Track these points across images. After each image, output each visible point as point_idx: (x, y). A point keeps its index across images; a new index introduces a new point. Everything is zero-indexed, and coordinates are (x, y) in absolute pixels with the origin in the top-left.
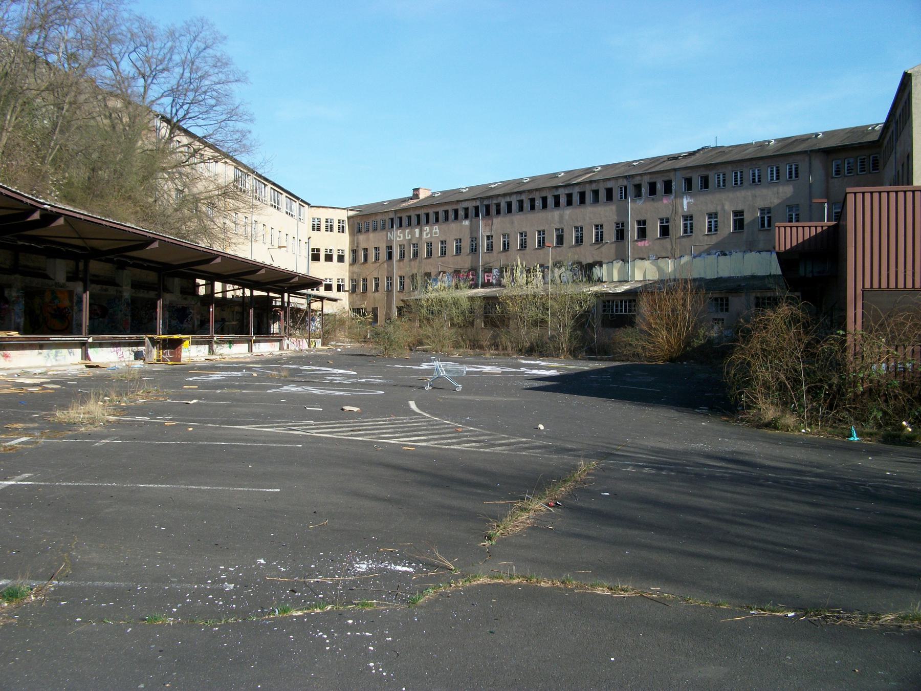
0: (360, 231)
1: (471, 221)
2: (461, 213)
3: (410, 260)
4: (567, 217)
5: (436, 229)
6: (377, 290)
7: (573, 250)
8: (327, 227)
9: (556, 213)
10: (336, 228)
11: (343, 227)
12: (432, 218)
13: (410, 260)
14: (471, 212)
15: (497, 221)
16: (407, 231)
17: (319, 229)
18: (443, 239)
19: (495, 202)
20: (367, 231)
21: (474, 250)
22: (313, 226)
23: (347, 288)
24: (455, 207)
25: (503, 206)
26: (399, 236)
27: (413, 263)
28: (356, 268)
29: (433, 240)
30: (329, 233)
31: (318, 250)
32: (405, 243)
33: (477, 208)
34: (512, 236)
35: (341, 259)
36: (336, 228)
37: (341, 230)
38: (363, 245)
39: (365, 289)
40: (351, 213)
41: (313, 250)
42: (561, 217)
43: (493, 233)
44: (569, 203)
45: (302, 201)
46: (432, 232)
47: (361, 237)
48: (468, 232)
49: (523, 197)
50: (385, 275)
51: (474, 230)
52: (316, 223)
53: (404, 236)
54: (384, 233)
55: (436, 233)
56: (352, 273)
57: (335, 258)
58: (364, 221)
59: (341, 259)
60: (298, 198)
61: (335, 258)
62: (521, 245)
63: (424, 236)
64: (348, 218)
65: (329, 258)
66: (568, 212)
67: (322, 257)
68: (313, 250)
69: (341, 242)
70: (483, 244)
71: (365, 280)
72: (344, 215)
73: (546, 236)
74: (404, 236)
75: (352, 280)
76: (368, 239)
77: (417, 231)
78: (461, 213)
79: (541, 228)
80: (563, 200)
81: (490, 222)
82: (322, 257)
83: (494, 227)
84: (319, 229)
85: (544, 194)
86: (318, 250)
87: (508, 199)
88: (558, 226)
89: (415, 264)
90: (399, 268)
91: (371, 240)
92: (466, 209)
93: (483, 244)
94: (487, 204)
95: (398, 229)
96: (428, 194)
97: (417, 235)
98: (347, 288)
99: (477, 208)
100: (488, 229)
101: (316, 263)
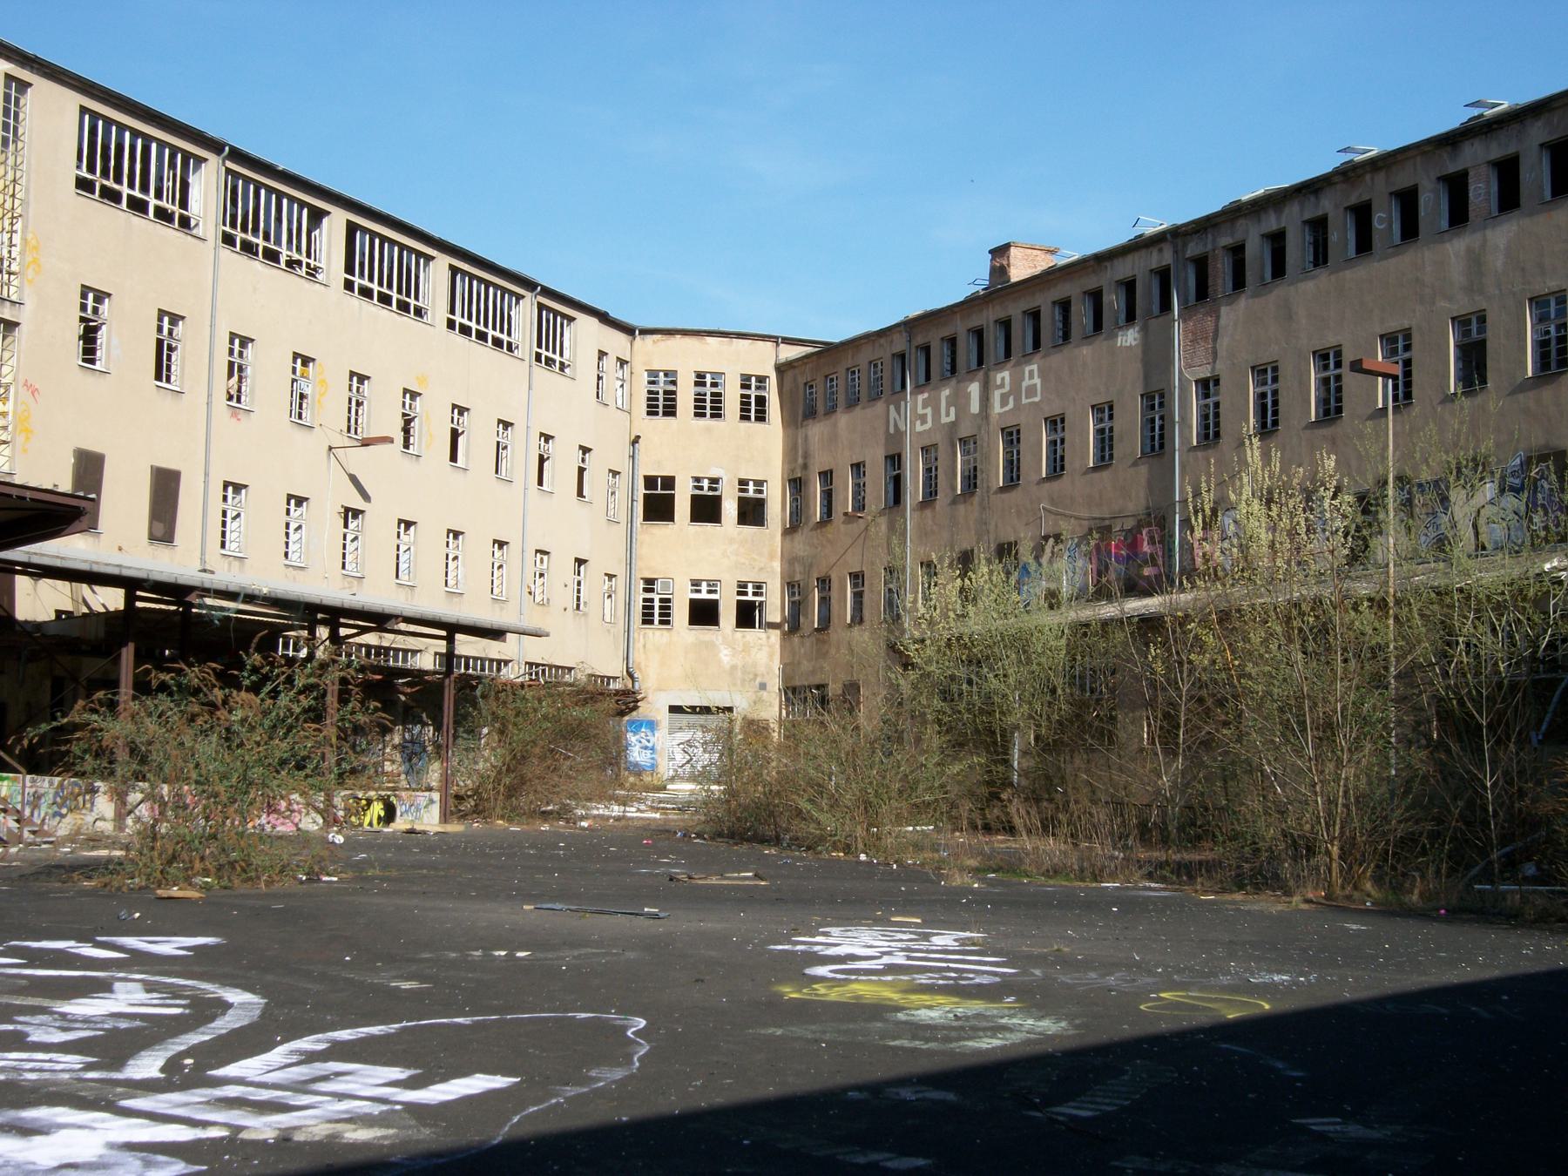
0: (811, 413)
1: (1145, 330)
2: (1113, 301)
3: (955, 501)
4: (1497, 262)
5: (1032, 374)
6: (858, 618)
7: (1527, 399)
8: (699, 401)
9: (1457, 247)
10: (732, 404)
11: (761, 401)
12: (1022, 333)
13: (955, 501)
14: (1147, 294)
15: (1234, 315)
16: (946, 393)
17: (670, 411)
18: (1053, 410)
19: (1226, 240)
20: (831, 410)
21: (1157, 444)
22: (652, 398)
23: (774, 613)
24: (1091, 283)
25: (1256, 251)
26: (923, 414)
27: (961, 508)
28: (800, 544)
29: (1023, 420)
30: (753, 426)
31: (669, 482)
32: (938, 438)
33: (1164, 276)
34: (1286, 371)
35: (751, 512)
36: (732, 404)
37: (754, 410)
38: (819, 462)
39: (826, 622)
40: (790, 353)
41: (650, 482)
42: (1475, 262)
43: (1221, 368)
44: (1509, 200)
45: (547, 292)
46: (1018, 389)
47: (816, 431)
48: (1134, 370)
49: (1327, 205)
50: (882, 560)
51: (1156, 358)
52: (661, 387)
53: (936, 412)
54: (880, 406)
55: (1031, 391)
56: (789, 560)
57: (730, 508)
58: (822, 382)
59: (751, 512)
60: (530, 285)
61: (730, 508)
62: (1324, 402)
63: (997, 408)
64: (781, 369)
65: (707, 509)
66: (1501, 238)
67: (682, 507)
68: (650, 482)
69: (756, 453)
70: (1188, 413)
71: (824, 583)
72: (763, 360)
73: (1415, 353)
74: (936, 412)
75: (791, 586)
76: (833, 438)
77: (974, 389)
78: (1113, 301)
79: (1393, 325)
80: (1482, 190)
81: (1209, 323)
82: (682, 507)
83: (1224, 343)
84: (670, 411)
85: (1402, 180)
86: (669, 482)
87: (1271, 223)
88: (1463, 306)
89: (968, 513)
90: (923, 534)
91: (848, 437)
92: (1129, 286)
93: (1188, 413)
94: (1199, 264)
95: (918, 388)
96: (1042, 263)
97: (975, 407)
98: (774, 613)
99: (1164, 276)
100: (1202, 350)
101: (660, 530)
